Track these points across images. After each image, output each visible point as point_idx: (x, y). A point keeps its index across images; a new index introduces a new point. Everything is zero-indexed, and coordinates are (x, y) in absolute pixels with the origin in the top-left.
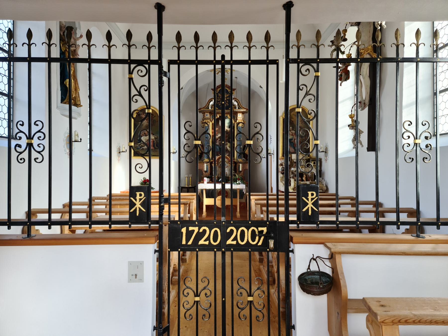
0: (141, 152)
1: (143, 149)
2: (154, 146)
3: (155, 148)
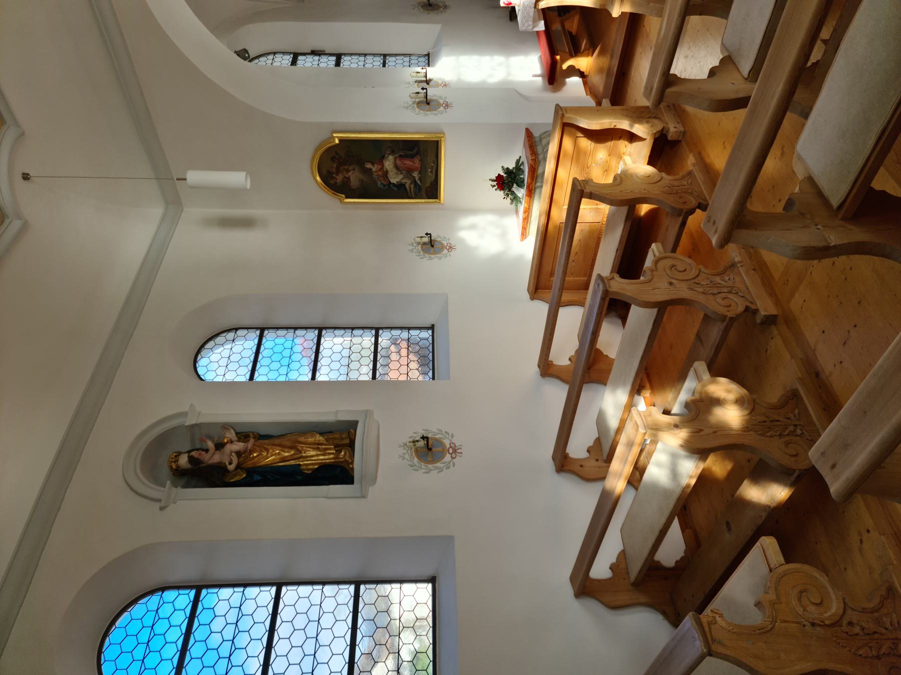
0: (428, 185)
1: (420, 179)
2: (412, 157)
3: (418, 153)
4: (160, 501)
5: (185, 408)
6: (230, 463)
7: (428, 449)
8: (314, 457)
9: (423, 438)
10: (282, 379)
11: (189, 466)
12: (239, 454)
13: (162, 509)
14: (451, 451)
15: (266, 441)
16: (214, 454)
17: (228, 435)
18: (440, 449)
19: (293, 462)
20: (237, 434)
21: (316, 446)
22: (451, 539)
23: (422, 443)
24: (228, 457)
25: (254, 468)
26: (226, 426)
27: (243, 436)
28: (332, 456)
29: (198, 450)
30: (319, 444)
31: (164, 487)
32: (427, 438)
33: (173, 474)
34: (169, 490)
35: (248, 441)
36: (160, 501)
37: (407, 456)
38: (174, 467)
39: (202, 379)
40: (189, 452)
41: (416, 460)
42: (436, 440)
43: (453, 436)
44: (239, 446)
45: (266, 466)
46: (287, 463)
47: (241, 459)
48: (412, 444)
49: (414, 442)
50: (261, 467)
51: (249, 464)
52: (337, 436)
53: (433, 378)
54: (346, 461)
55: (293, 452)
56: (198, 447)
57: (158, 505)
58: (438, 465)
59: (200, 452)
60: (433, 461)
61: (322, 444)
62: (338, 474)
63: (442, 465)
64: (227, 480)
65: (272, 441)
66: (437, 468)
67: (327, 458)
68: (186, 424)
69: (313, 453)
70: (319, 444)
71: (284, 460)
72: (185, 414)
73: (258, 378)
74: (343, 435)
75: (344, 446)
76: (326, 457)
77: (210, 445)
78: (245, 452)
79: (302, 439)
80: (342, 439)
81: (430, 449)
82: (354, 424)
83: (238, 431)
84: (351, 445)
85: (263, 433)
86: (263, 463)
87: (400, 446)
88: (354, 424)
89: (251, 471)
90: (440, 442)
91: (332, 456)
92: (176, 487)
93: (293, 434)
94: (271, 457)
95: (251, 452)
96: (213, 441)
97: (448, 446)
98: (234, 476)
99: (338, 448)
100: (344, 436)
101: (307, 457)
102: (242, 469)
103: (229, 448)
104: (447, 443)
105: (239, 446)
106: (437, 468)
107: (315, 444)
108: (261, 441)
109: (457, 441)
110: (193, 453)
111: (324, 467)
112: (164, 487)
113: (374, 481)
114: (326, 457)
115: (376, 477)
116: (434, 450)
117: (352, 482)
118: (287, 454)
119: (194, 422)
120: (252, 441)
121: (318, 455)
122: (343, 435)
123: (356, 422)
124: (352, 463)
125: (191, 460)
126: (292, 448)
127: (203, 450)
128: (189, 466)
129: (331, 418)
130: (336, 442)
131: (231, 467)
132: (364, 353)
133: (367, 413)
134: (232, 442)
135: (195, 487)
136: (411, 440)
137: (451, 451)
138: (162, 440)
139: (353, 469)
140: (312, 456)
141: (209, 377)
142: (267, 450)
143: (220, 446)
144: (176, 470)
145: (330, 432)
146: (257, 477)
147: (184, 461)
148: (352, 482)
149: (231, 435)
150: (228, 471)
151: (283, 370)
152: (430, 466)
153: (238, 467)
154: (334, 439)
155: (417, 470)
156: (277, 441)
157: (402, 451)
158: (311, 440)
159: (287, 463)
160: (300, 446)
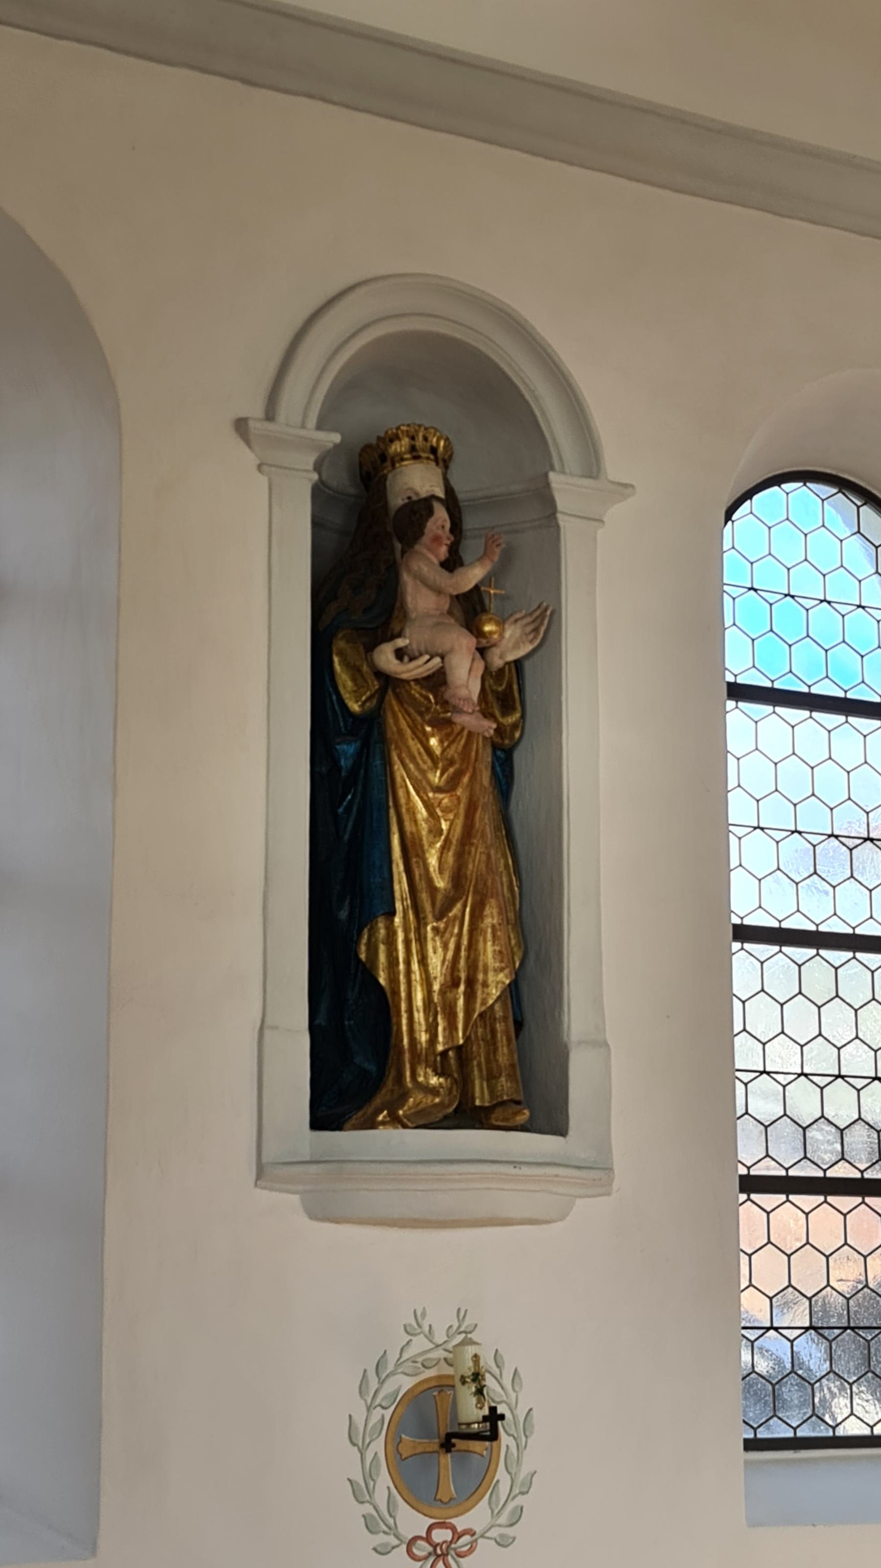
4: (270, 415)
5: (615, 466)
6: (400, 654)
7: (448, 1433)
8: (422, 968)
9: (494, 1417)
10: (739, 810)
11: (397, 501)
12: (437, 681)
13: (241, 426)
14: (441, 1536)
15: (485, 777)
16: (439, 592)
17: (511, 632)
18: (449, 1488)
19: (401, 886)
20: (518, 664)
21: (465, 975)
22: (93, 1549)
23: (471, 1411)
24: (432, 644)
25: (383, 740)
26: (546, 623)
27: (509, 691)
28: (423, 1037)
29: (456, 528)
30: (471, 983)
31: (319, 427)
32: (494, 1436)
33: (367, 448)
34: (307, 442)
35: (487, 714)
36: (270, 415)
37: (420, 1344)
38: (397, 447)
39: (729, 516)
40: (451, 501)
41: (406, 1383)
42: (489, 1469)
43: (503, 1543)
44: (466, 679)
45: (389, 784)
46: (398, 866)
47: (416, 691)
48: (467, 1367)
49: (477, 1377)
50: (387, 763)
51: (398, 721)
52: (503, 1056)
53: (751, 1445)
54: (404, 1096)
55: (440, 883)
56: (470, 522)
57: (255, 409)
58: (384, 1480)
59: (447, 539)
60: (397, 1460)
61: (470, 996)
62: (354, 1064)
63: (381, 1498)
64: (340, 644)
65: (487, 799)
66: (370, 1476)
67: (416, 1022)
68: (552, 476)
69: (436, 962)
70: (471, 983)
71: (412, 851)
72: (592, 465)
73: (739, 718)
74: (509, 1076)
75: (464, 1084)
76: (419, 1016)
77: (472, 575)
78: (445, 704)
79: (491, 917)
80: (491, 1077)
81: (447, 1445)
82: (551, 1120)
83: (528, 666)
84: (466, 1115)
85: (518, 757)
86: (399, 772)
87: (461, 1315)
88: (551, 1120)
89: (370, 731)
90: (477, 1486)
91: (423, 1037)
92: (318, 467)
93: (516, 874)
94: (425, 807)
95: (442, 724)
96: (487, 580)
97: (461, 1524)
98: (355, 671)
99: (457, 1063)
100: (504, 1082)
101: (422, 940)
102: (382, 694)
103: (461, 645)
104: (476, 1517)
105: (466, 679)
106: (370, 1476)
107: (473, 967)
108: (487, 756)
109: (394, 426)
110: (441, 514)
111: (380, 1007)
112: (319, 427)
113: (321, 1211)
114: (419, 1016)
115: (337, 1221)
116: (447, 1459)
117: (319, 1122)
118: (433, 861)
119: (561, 503)
120: (488, 727)
121: (427, 982)
122: (509, 1076)
123: (561, 1130)
124: (396, 1121)
125: (421, 508)
126: (458, 880)
127: (454, 549)
128: (397, 501)
129: (577, 1020)
130: (479, 1053)
131: (386, 657)
132: (828, 1240)
133: (598, 1171)
134: (482, 651)
135: (316, 524)
136: (487, 1361)
137: (441, 1536)
138: (490, 393)
139: (372, 1125)
140: (423, 961)
141: (746, 530)
142: (450, 786)
143: (470, 609)
144: (383, 457)
145: (519, 1025)
146: (348, 750)
147: (418, 480)
148: (319, 1122)
149: (511, 642)
150: (371, 647)
151: (776, 814)
152: (378, 1446)
153: (387, 681)
154: (492, 1044)
155: (362, 1391)
156: (485, 820)
157: (441, 1322)
158: (489, 951)
159: (398, 866)
160: (463, 910)
